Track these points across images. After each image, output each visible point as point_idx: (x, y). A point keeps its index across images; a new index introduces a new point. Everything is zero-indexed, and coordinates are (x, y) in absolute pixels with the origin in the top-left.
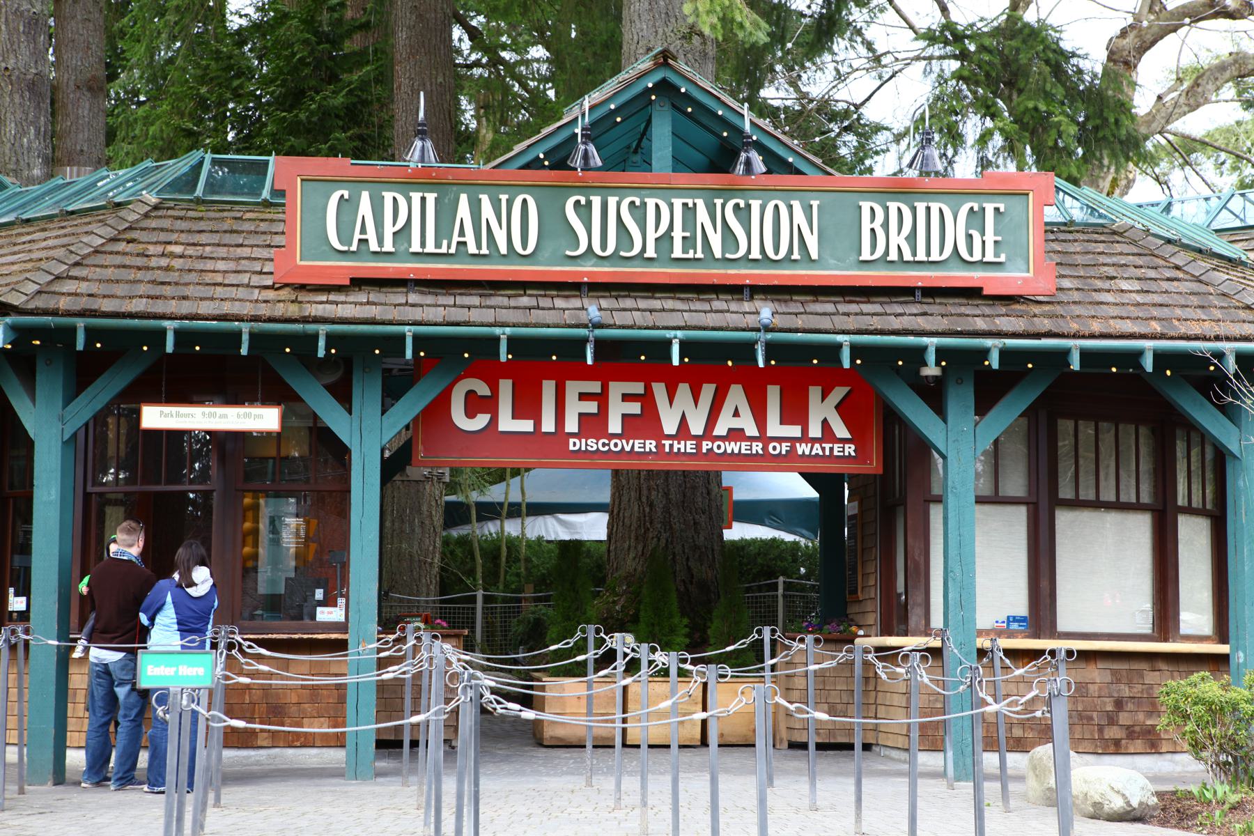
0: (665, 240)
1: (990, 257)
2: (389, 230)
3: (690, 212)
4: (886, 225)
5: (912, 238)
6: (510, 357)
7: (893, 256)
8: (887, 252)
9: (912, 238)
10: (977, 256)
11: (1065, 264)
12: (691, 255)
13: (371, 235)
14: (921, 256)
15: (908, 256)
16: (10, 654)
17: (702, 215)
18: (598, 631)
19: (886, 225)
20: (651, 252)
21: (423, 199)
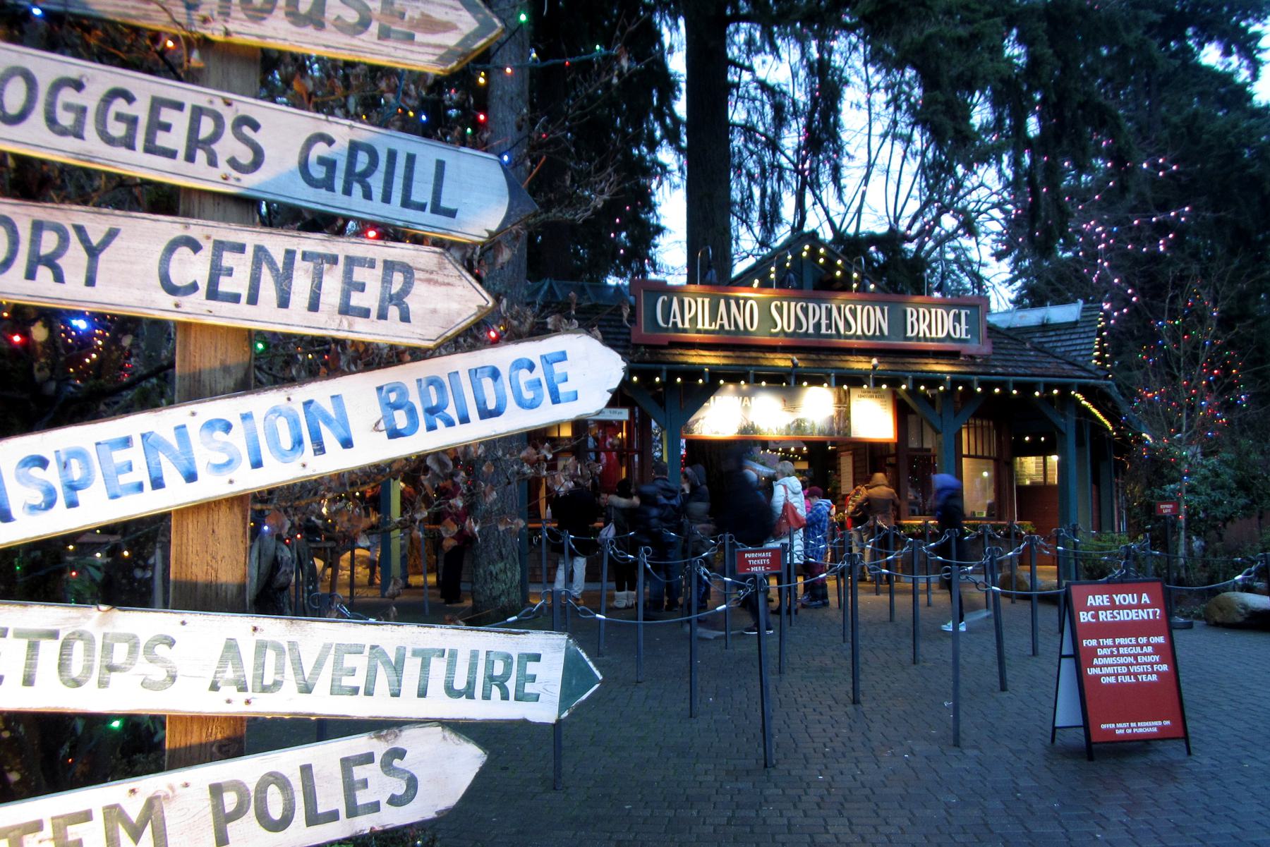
0: (818, 326)
1: (964, 336)
2: (687, 317)
3: (829, 312)
4: (918, 319)
5: (929, 326)
6: (722, 382)
7: (921, 335)
8: (918, 333)
9: (929, 326)
10: (958, 336)
11: (995, 345)
12: (829, 332)
13: (679, 320)
14: (934, 335)
15: (928, 335)
16: (34, 675)
17: (835, 313)
18: (731, 538)
19: (918, 319)
20: (811, 331)
21: (703, 302)
